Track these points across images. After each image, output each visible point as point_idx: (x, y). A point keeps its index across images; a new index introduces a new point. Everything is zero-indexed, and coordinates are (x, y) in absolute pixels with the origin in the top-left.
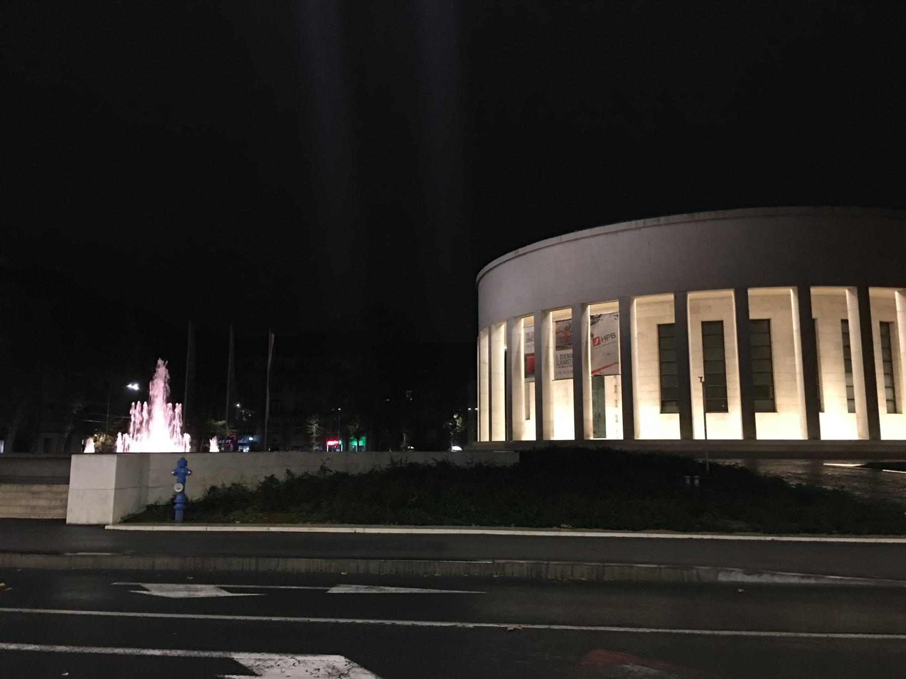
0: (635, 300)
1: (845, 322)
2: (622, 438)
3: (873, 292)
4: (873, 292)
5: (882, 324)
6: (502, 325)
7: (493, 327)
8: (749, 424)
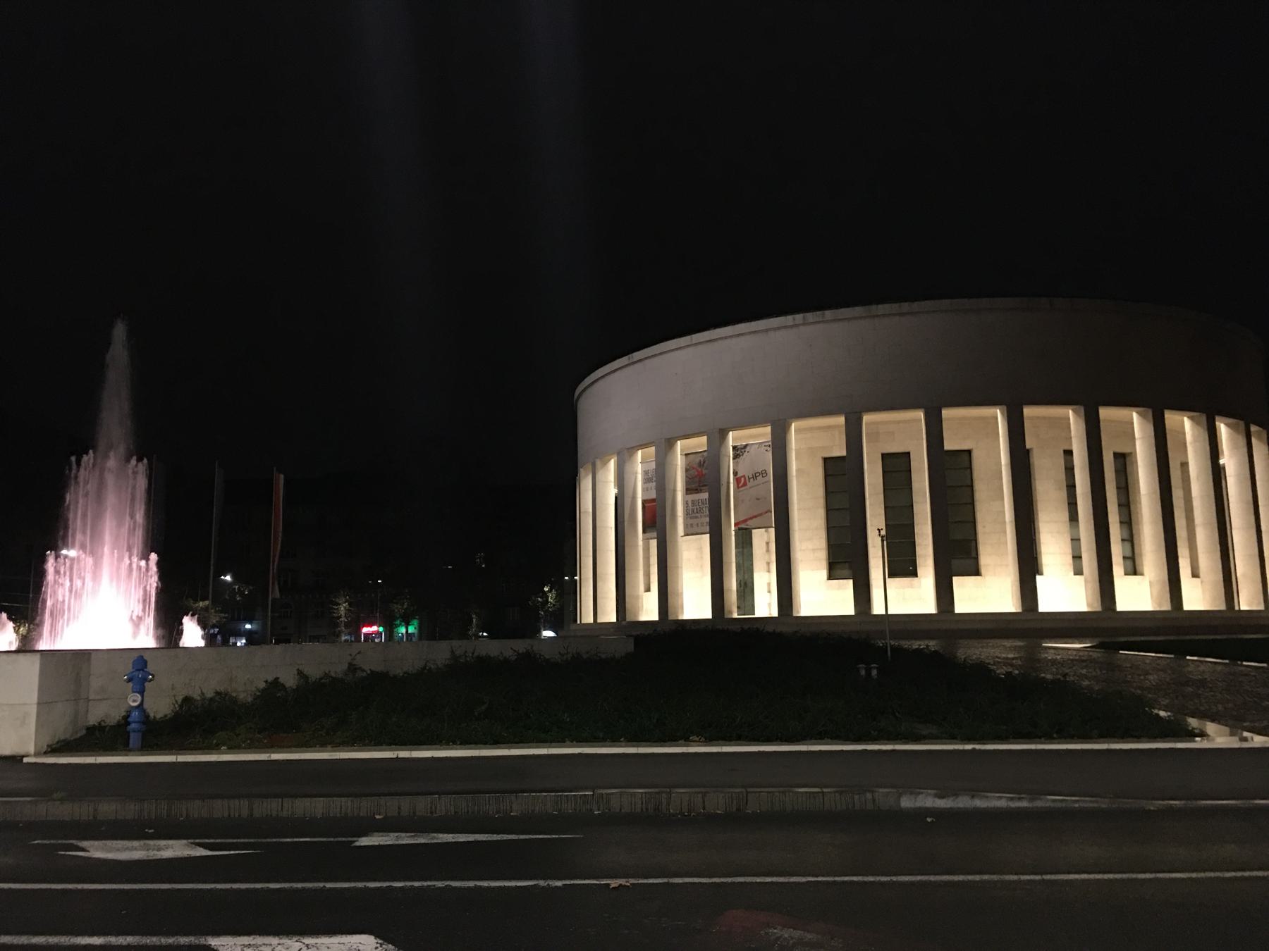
0: (793, 424)
1: (1068, 453)
3: (1105, 413)
4: (1105, 413)
5: (1117, 455)
6: (611, 459)
7: (598, 463)
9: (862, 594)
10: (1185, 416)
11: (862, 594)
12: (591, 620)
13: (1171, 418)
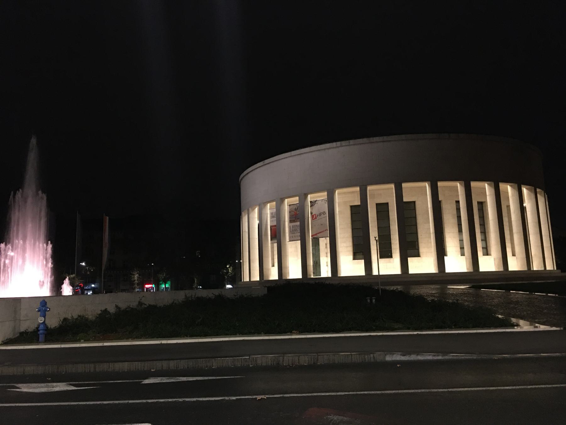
1: (458, 202)
2: (278, 279)
3: (473, 184)
4: (473, 184)
5: (479, 203)
7: (250, 209)
8: (404, 265)
9: (368, 266)
10: (508, 185)
11: (368, 266)
12: (248, 280)
13: (502, 186)
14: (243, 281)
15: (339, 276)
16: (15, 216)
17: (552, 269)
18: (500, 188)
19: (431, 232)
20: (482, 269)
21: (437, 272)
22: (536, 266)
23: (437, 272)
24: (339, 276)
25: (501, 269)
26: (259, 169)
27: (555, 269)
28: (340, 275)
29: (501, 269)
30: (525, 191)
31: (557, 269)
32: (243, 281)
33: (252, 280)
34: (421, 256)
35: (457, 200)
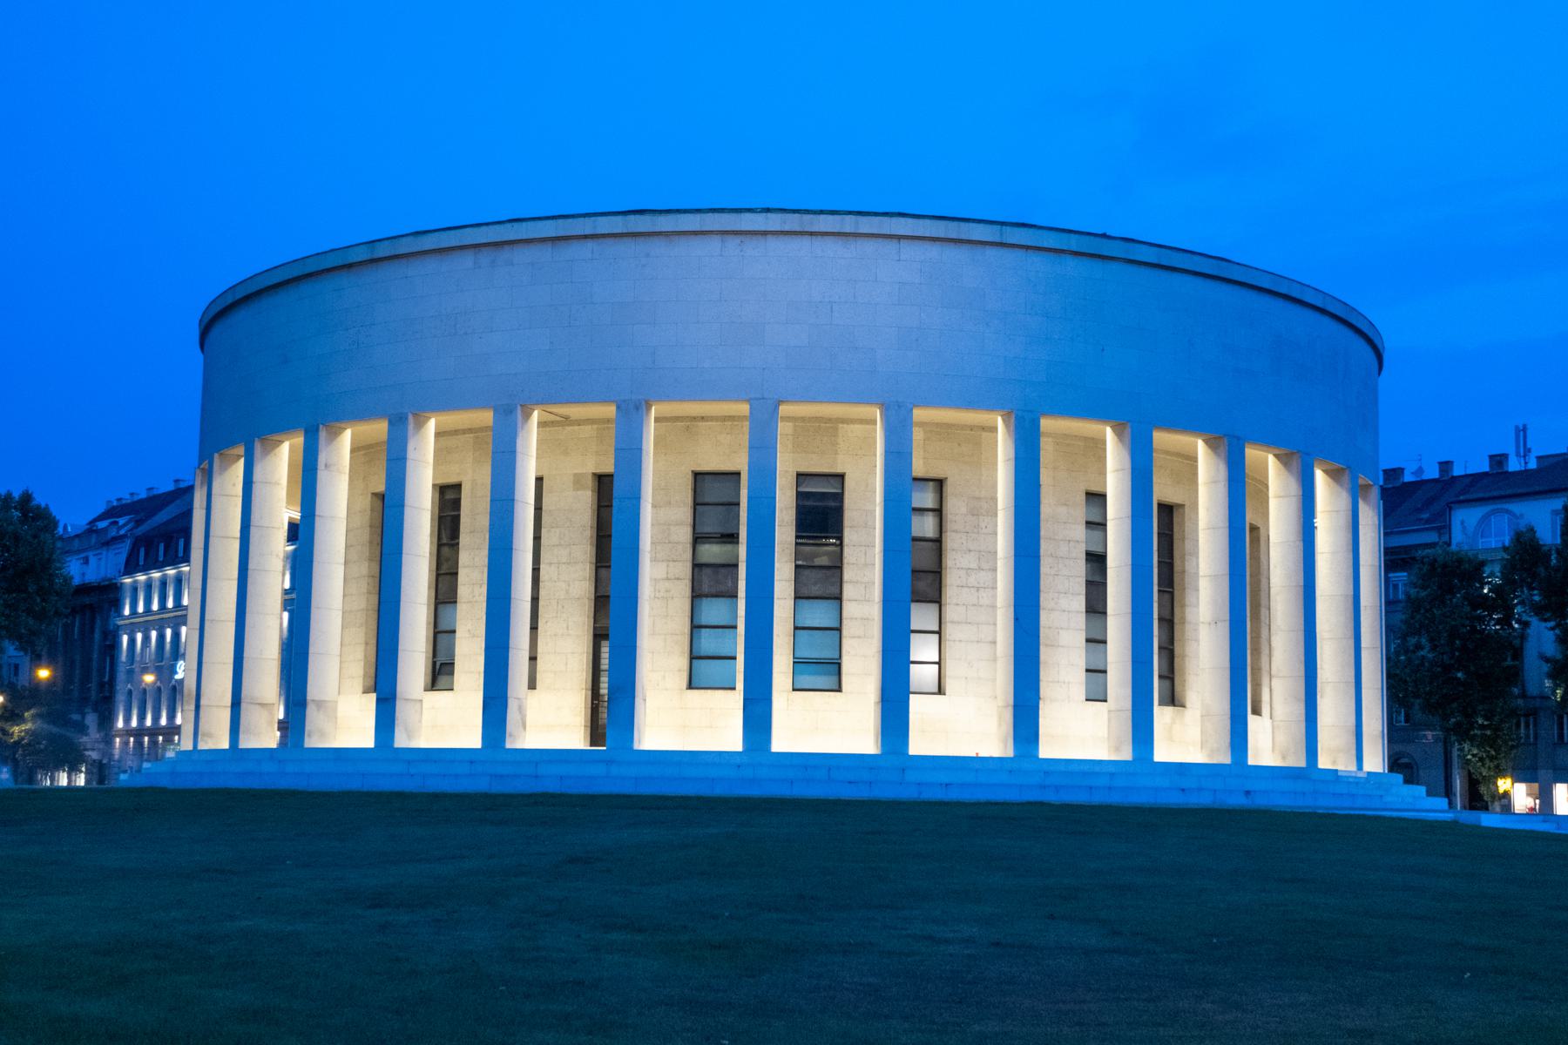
1: (1097, 498)
5: (1161, 506)
13: (1252, 453)
14: (293, 725)
15: (636, 747)
16: (120, 632)
17: (1382, 771)
18: (1247, 455)
19: (999, 605)
20: (1047, 750)
21: (1010, 753)
22: (1333, 756)
23: (1010, 753)
24: (636, 747)
25: (1224, 758)
26: (590, 244)
27: (1386, 771)
28: (322, 734)
29: (1224, 758)
30: (1320, 476)
31: (604, 746)
32: (293, 725)
33: (401, 741)
34: (947, 692)
35: (1095, 488)
